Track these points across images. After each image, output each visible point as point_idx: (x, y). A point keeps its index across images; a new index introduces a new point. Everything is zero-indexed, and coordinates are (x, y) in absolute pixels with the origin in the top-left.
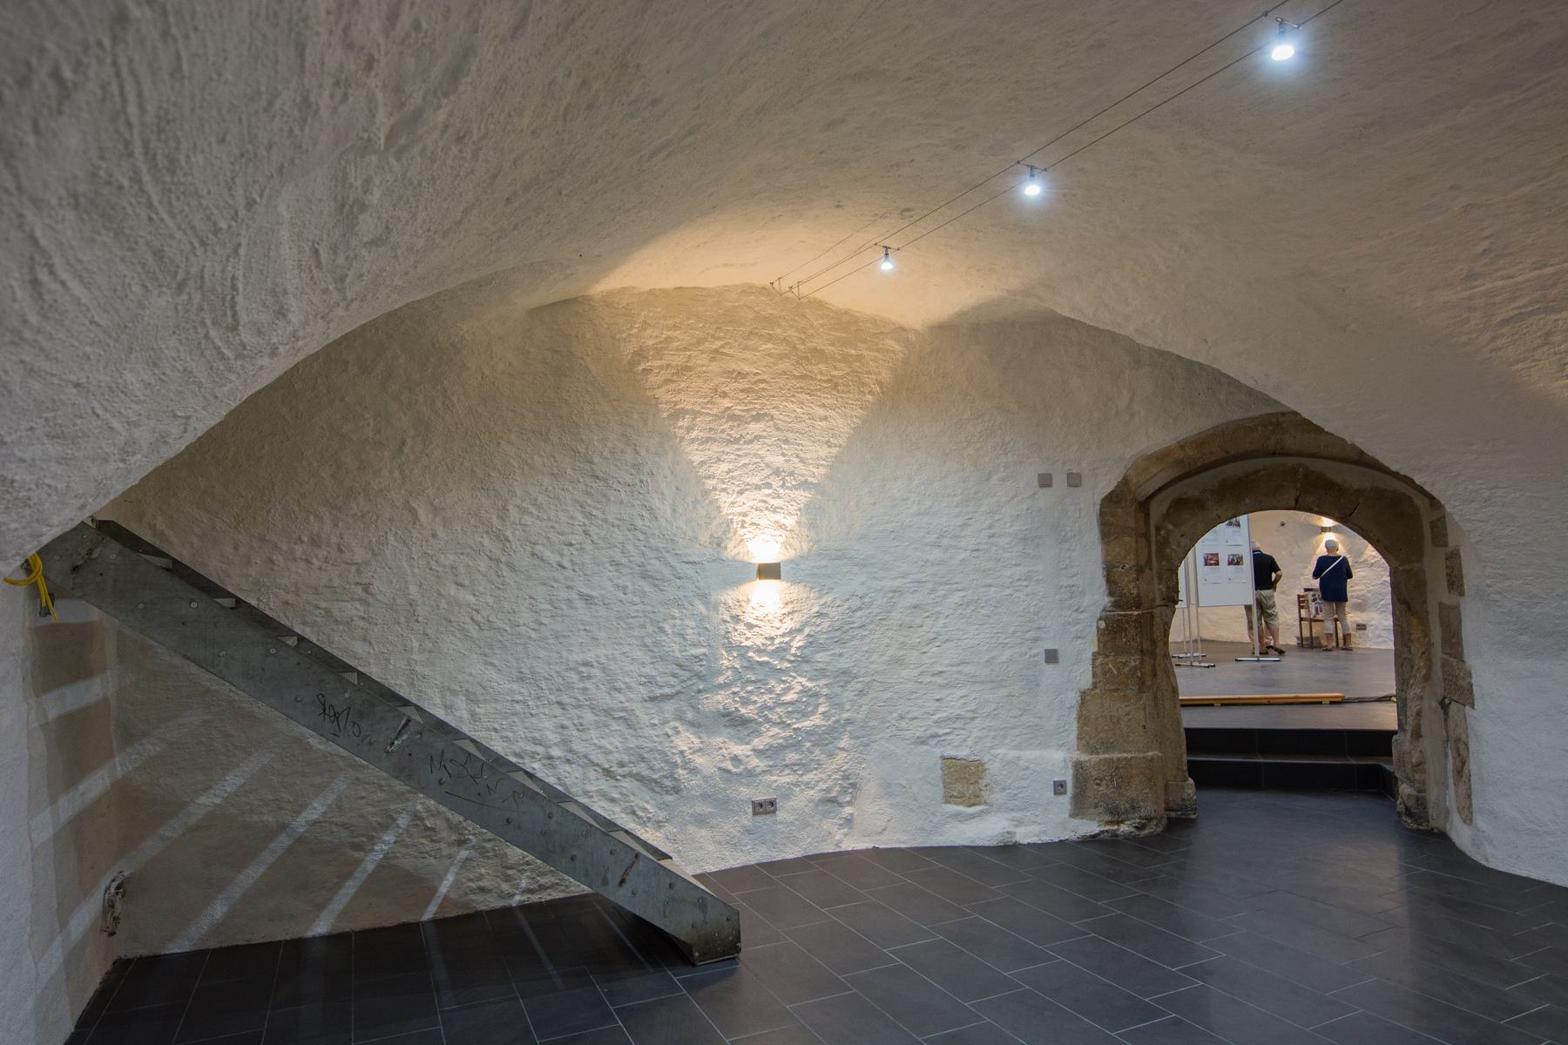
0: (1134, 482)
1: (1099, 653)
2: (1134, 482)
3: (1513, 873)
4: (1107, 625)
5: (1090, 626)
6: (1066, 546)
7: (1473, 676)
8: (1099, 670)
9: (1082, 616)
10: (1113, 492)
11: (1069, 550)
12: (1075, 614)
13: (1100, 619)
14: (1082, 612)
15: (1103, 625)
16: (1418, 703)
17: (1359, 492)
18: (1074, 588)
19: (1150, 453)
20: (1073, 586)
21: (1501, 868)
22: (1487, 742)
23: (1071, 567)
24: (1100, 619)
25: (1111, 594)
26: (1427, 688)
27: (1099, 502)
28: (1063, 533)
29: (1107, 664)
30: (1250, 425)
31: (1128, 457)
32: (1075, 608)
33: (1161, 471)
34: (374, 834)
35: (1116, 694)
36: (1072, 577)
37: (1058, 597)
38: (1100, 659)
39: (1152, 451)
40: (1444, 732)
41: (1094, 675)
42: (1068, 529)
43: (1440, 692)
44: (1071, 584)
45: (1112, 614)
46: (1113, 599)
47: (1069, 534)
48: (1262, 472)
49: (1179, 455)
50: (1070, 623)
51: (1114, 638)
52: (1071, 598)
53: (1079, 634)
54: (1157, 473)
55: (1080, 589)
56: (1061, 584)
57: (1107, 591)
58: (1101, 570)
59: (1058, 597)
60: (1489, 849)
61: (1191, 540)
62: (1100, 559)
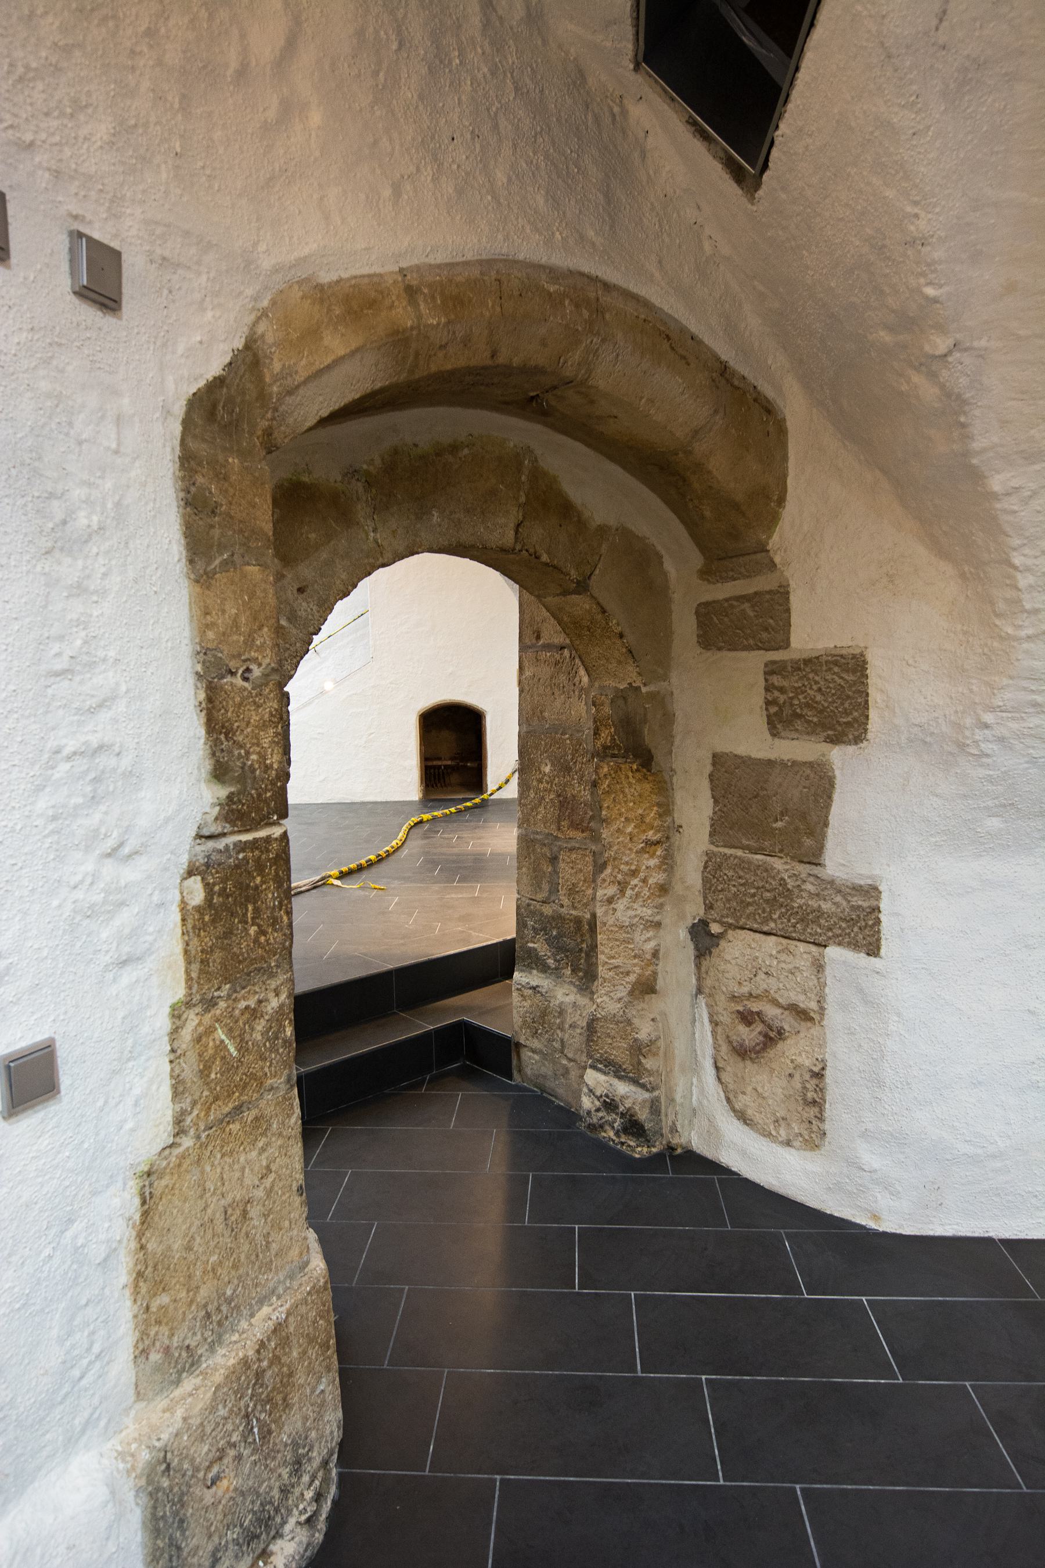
0: (277, 366)
1: (188, 1004)
2: (277, 366)
3: (931, 1233)
4: (208, 887)
5: (161, 905)
6: (69, 569)
7: (884, 896)
8: (190, 1068)
9: (131, 874)
10: (218, 382)
11: (79, 589)
12: (109, 869)
13: (190, 873)
14: (129, 856)
15: (197, 893)
16: (651, 934)
17: (603, 530)
18: (105, 761)
19: (326, 277)
20: (101, 748)
21: (908, 1229)
22: (899, 1015)
23: (92, 665)
24: (190, 873)
25: (220, 773)
26: (668, 908)
27: (179, 409)
28: (57, 509)
29: (210, 1031)
30: (552, 289)
31: (266, 263)
32: (110, 843)
33: (353, 353)
34: (620, 335)
35: (235, 1127)
36: (92, 711)
37: (42, 804)
38: (192, 1020)
39: (333, 277)
40: (694, 981)
41: (178, 1090)
42: (78, 493)
43: (695, 910)
44: (94, 740)
45: (220, 844)
46: (223, 792)
47: (82, 520)
48: (466, 451)
49: (403, 315)
50: (91, 913)
51: (228, 934)
52: (94, 800)
53: (126, 949)
54: (343, 358)
55: (126, 762)
56: (51, 744)
57: (208, 765)
58: (191, 680)
59: (42, 804)
60: (883, 1201)
61: (320, 605)
62: (187, 633)
